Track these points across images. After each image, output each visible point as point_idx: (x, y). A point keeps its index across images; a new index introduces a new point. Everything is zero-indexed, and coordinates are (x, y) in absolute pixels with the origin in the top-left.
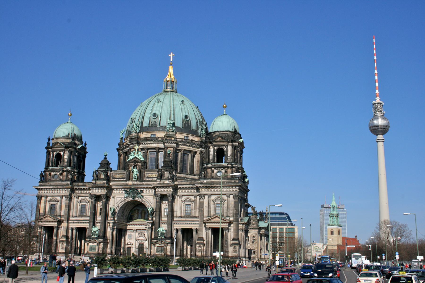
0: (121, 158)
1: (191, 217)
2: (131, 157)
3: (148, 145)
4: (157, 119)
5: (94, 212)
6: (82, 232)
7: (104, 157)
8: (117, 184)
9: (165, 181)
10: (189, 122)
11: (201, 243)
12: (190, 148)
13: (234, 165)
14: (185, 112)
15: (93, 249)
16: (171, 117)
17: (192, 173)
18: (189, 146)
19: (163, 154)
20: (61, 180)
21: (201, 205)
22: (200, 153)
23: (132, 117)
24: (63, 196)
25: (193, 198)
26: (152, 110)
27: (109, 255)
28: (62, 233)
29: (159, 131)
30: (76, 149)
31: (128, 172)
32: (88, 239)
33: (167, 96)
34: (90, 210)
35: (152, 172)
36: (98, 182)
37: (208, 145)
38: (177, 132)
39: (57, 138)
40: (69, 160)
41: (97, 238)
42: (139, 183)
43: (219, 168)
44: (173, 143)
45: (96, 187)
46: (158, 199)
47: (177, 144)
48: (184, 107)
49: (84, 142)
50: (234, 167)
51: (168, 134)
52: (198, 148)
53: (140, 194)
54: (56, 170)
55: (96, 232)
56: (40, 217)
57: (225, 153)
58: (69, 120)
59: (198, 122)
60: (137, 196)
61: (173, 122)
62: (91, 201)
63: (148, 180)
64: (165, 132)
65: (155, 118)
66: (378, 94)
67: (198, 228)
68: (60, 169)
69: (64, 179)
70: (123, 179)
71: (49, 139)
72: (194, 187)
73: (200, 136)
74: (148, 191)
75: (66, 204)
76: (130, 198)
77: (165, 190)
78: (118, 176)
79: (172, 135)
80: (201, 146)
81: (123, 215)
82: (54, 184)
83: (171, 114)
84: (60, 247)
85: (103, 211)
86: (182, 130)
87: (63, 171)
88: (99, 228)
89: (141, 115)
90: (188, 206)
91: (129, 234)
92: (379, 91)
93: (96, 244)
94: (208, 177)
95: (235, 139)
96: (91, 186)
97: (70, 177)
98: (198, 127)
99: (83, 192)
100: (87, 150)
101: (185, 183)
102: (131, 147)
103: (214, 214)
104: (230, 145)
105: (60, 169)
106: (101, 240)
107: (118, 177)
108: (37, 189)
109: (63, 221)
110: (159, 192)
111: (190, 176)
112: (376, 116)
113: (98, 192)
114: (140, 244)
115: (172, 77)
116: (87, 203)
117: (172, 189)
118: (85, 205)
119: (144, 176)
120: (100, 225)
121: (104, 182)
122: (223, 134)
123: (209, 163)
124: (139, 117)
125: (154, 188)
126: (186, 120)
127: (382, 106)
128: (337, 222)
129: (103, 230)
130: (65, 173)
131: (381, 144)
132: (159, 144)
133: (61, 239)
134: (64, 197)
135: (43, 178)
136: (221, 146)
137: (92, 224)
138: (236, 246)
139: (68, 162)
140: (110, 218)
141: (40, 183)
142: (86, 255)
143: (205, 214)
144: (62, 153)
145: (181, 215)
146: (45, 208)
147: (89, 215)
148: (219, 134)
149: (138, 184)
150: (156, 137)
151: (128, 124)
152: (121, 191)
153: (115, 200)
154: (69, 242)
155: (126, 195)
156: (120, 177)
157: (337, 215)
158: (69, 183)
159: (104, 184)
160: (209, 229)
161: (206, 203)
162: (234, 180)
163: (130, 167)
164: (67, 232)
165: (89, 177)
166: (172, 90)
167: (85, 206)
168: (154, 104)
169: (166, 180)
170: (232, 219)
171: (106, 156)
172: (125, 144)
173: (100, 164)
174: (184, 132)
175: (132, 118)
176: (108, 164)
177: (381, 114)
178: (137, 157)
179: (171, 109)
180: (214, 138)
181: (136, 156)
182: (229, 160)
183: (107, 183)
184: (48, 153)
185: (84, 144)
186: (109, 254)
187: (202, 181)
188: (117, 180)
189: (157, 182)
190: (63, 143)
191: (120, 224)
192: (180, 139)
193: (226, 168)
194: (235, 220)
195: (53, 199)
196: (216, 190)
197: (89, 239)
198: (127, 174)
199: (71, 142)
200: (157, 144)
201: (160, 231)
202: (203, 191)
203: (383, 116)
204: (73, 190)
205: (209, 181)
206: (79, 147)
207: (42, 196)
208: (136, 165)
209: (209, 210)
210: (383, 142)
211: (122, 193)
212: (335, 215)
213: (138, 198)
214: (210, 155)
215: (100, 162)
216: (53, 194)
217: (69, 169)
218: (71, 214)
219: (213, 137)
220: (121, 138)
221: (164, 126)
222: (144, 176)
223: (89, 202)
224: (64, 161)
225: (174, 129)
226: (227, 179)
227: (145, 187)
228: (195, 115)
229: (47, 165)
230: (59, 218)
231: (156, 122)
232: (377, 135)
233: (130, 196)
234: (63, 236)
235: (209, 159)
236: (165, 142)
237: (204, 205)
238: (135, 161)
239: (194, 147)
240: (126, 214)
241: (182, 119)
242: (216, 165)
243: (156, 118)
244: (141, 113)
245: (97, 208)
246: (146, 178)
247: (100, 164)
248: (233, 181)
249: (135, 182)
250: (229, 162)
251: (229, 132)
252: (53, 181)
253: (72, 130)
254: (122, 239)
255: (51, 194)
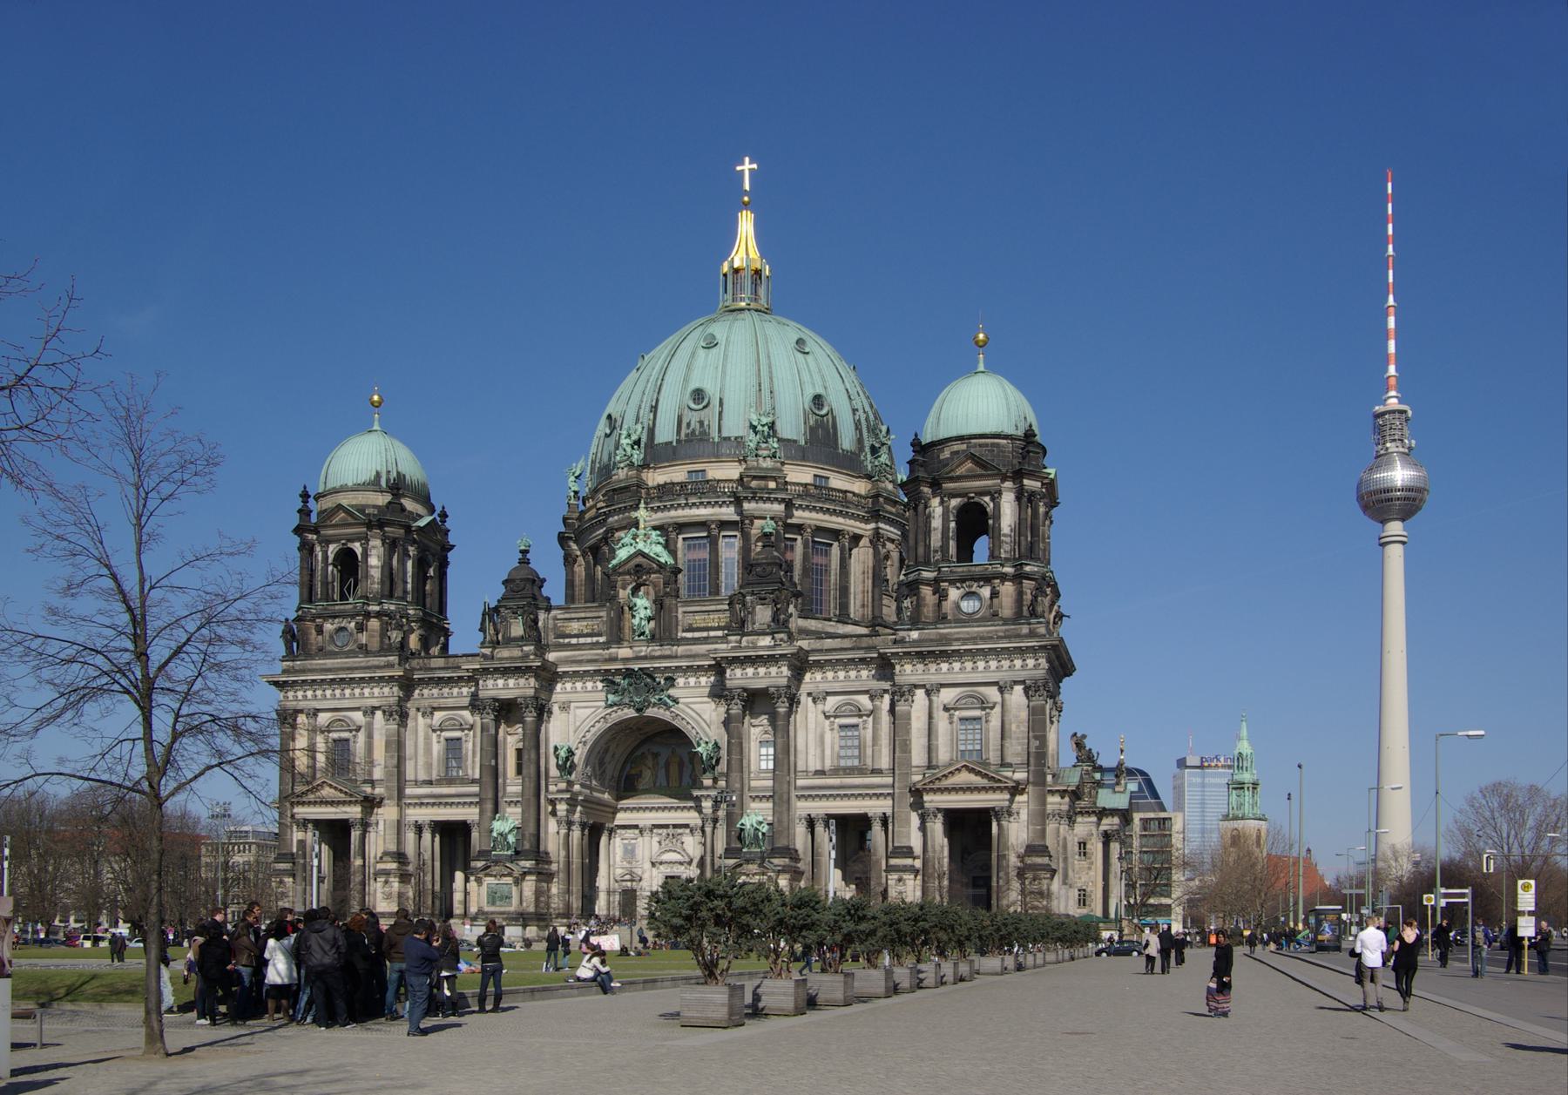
0: (576, 568)
1: (860, 771)
2: (622, 554)
3: (680, 512)
4: (706, 410)
5: (493, 762)
6: (453, 836)
7: (520, 556)
8: (574, 656)
9: (761, 637)
10: (828, 421)
11: (905, 869)
12: (834, 518)
13: (1027, 569)
14: (814, 385)
15: (501, 898)
16: (761, 402)
17: (844, 618)
18: (834, 513)
19: (737, 544)
20: (364, 650)
21: (899, 722)
22: (871, 541)
23: (613, 408)
24: (374, 709)
25: (864, 701)
26: (686, 380)
27: (559, 920)
28: (381, 842)
29: (717, 457)
30: (408, 529)
31: (612, 609)
32: (480, 864)
33: (737, 324)
34: (478, 759)
35: (704, 609)
36: (504, 653)
37: (921, 492)
38: (787, 458)
39: (336, 491)
40: (387, 573)
41: (512, 859)
42: (656, 650)
43: (968, 580)
44: (776, 499)
45: (496, 670)
46: (736, 707)
47: (789, 505)
48: (806, 362)
49: (438, 509)
50: (1028, 577)
51: (755, 468)
52: (867, 522)
53: (662, 691)
54: (340, 611)
55: (506, 839)
56: (299, 789)
57: (991, 522)
58: (376, 423)
59: (863, 421)
60: (653, 700)
61: (769, 420)
62: (482, 724)
63: (693, 639)
64: (740, 461)
65: (701, 406)
66: (1393, 381)
67: (889, 812)
68: (355, 607)
69: (375, 645)
70: (595, 639)
71: (305, 496)
72: (871, 658)
73: (869, 477)
74: (692, 680)
75: (387, 736)
76: (626, 710)
77: (762, 674)
78: (575, 627)
79: (767, 469)
80: (879, 510)
81: (601, 774)
82: (336, 666)
83: (760, 390)
84: (379, 895)
85: (529, 759)
86: (803, 452)
87: (368, 615)
88: (517, 823)
89: (645, 400)
90: (850, 733)
91: (625, 844)
92: (1397, 370)
93: (509, 880)
94: (926, 617)
95: (1029, 464)
96: (478, 667)
97: (395, 636)
98: (860, 441)
99: (446, 690)
100: (452, 539)
101: (834, 646)
102: (616, 521)
103: (952, 760)
104: (1010, 490)
105: (355, 607)
106: (528, 864)
107: (575, 632)
108: (276, 684)
109: (382, 799)
110: (740, 681)
111: (840, 625)
112: (1380, 456)
113: (506, 687)
114: (667, 877)
115: (754, 254)
116: (466, 732)
117: (789, 669)
118: (459, 739)
119: (677, 625)
120: (519, 810)
121: (525, 648)
122: (980, 445)
123: (927, 563)
124: (640, 407)
125: (719, 668)
126: (817, 412)
127: (1407, 420)
128: (1254, 805)
129: (531, 829)
130: (374, 624)
131: (1395, 554)
132: (721, 506)
133: (380, 866)
134: (379, 714)
135: (295, 644)
136: (976, 494)
137: (489, 806)
138: (905, 877)
139: (382, 582)
140: (555, 787)
141: (288, 663)
142: (474, 919)
143: (918, 757)
144: (357, 547)
145: (823, 766)
146: (311, 750)
147: (477, 776)
148: (964, 447)
149: (653, 653)
150: (708, 481)
151: (595, 441)
152: (589, 685)
153: (571, 716)
154: (411, 875)
155: (611, 698)
156: (585, 631)
157: (1255, 785)
158: (393, 659)
159: (525, 656)
160: (936, 816)
161: (918, 718)
162: (1029, 624)
163: (621, 591)
164: (398, 838)
165: (465, 633)
166: (753, 305)
167: (461, 743)
168: (693, 354)
169: (764, 634)
170: (1020, 775)
171: (525, 552)
172: (587, 516)
173: (505, 582)
174: (814, 462)
175: (609, 417)
176: (537, 582)
177: (1401, 450)
178: (646, 551)
179: (759, 370)
180: (945, 463)
181: (641, 546)
182: (1007, 547)
183: (536, 655)
184: (307, 549)
185: (439, 516)
186: (559, 915)
187: (901, 634)
188: (574, 641)
189: (727, 642)
190: (361, 509)
191: (594, 806)
192: (798, 484)
193: (997, 578)
194: (1034, 777)
195: (340, 720)
196: (957, 666)
197: (484, 863)
198: (611, 620)
199: (390, 503)
200: (713, 506)
201: (748, 827)
202: (908, 672)
203: (1408, 455)
204: (407, 685)
205: (931, 633)
206: (422, 523)
207: (298, 711)
208: (645, 580)
209: (934, 742)
210: (1403, 543)
211: (595, 690)
212: (1246, 786)
213: (655, 709)
214: (930, 531)
215: (506, 578)
216: (336, 702)
217: (391, 607)
218: (410, 775)
219: (940, 461)
220: (572, 494)
221: (736, 438)
222: (674, 624)
223: (472, 727)
224: (367, 576)
225: (776, 445)
226: (1001, 623)
227: (684, 663)
228: (849, 397)
229: (306, 595)
230: (368, 790)
231: (706, 423)
232: (1383, 522)
233: (627, 700)
234: (386, 853)
235: (928, 547)
236: (746, 498)
237: (910, 724)
238: (637, 566)
239: (852, 517)
240: (612, 769)
241: (805, 413)
242: (955, 569)
243: (705, 407)
244: (644, 393)
245: (505, 749)
246: (684, 631)
247: (505, 582)
248: (1025, 630)
249: (644, 648)
250: (1008, 556)
251: (1006, 437)
252: (333, 655)
253: (389, 457)
254: (36, 1079)
255: (332, 702)
